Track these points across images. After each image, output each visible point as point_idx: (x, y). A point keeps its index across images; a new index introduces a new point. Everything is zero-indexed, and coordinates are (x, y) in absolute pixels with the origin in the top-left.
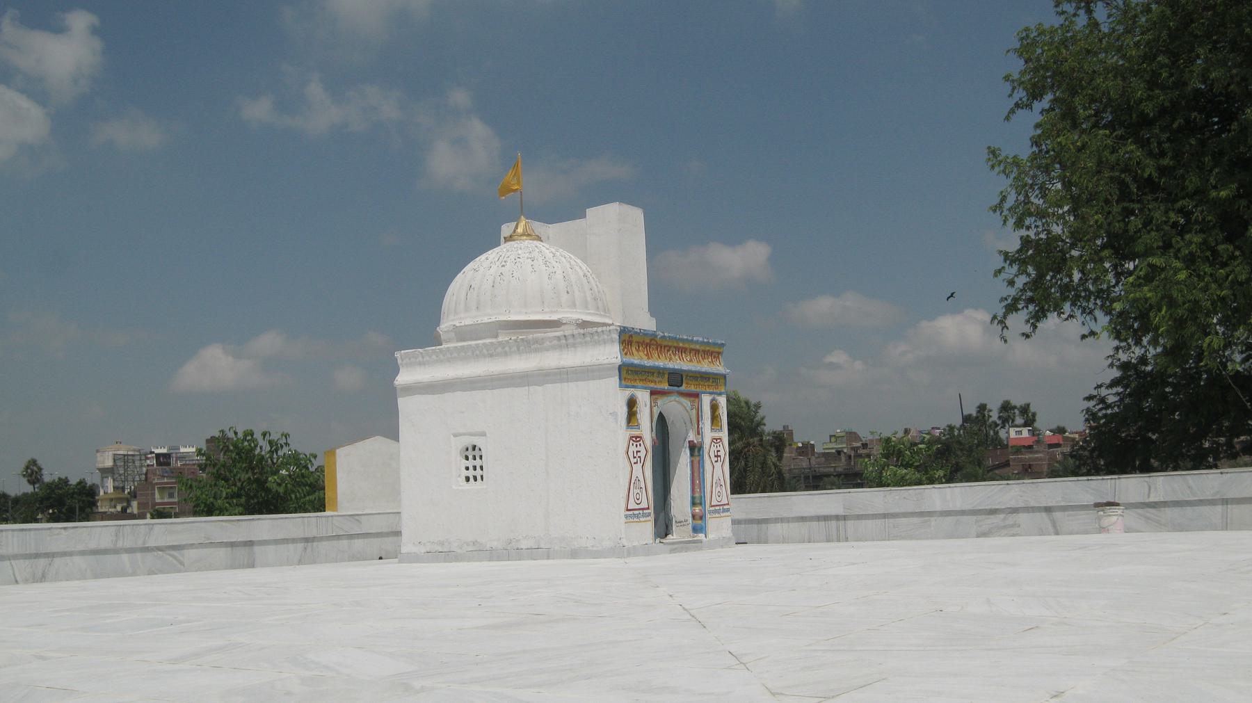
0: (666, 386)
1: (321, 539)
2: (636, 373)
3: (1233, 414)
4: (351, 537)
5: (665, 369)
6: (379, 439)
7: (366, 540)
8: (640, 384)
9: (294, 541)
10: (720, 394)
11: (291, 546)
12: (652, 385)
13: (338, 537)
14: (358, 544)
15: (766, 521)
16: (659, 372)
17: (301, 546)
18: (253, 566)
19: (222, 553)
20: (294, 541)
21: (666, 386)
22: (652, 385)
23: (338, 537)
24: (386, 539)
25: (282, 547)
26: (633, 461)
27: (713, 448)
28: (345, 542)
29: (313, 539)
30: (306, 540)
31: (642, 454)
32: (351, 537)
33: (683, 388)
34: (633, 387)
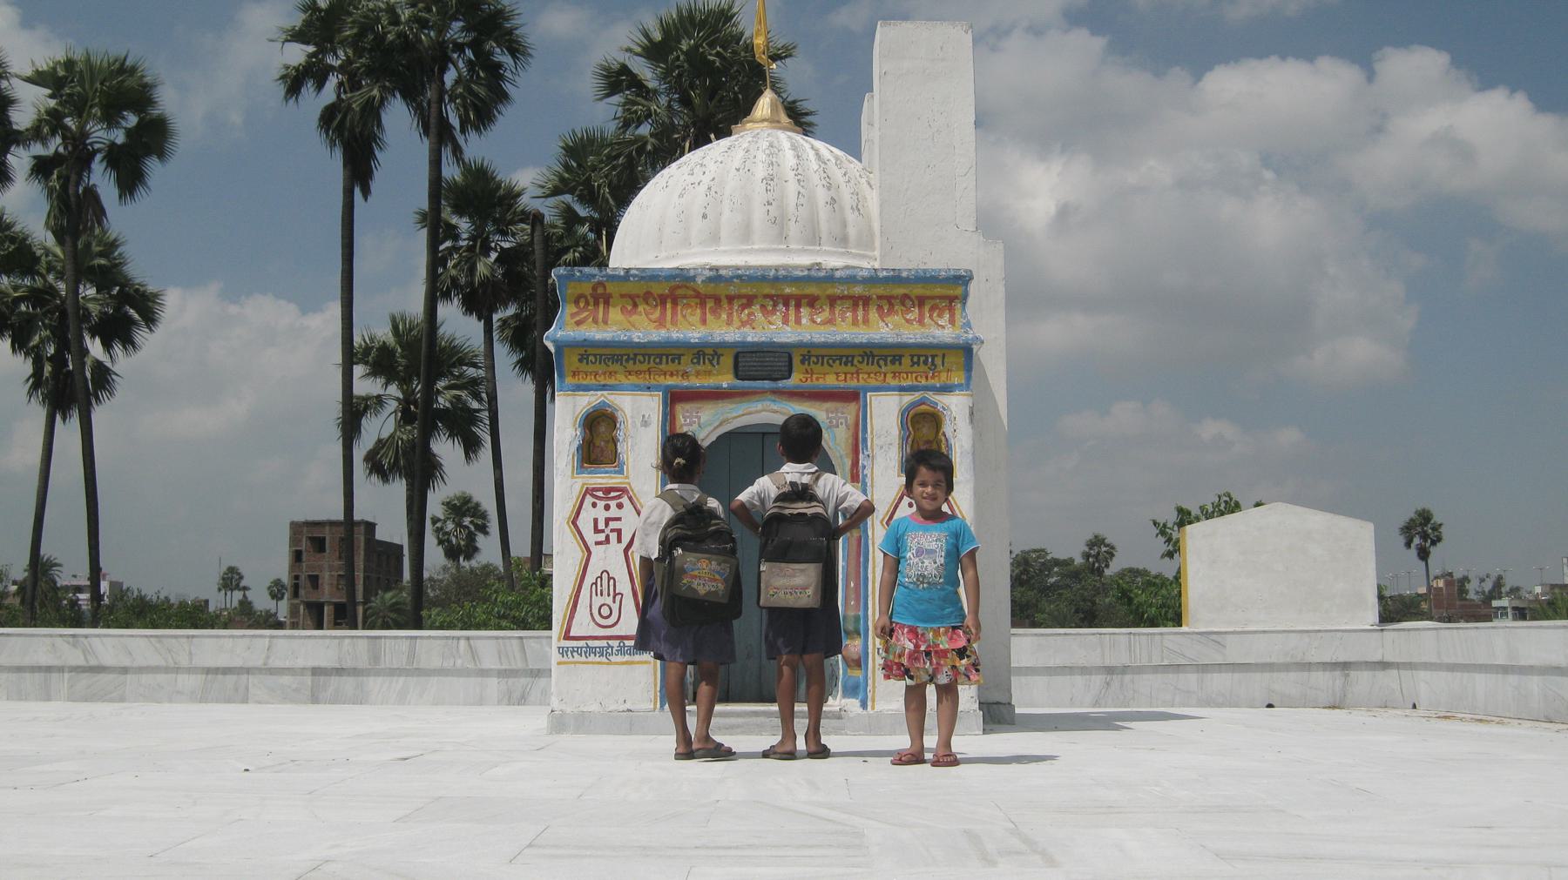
0: (726, 381)
1: (1140, 670)
2: (616, 359)
3: (1041, 189)
4: (1204, 668)
5: (724, 345)
7: (1237, 676)
8: (621, 378)
9: (1084, 670)
10: (946, 389)
11: (1079, 680)
13: (1177, 668)
14: (1219, 681)
17: (1098, 680)
20: (1084, 670)
21: (726, 381)
23: (1177, 668)
24: (1283, 675)
26: (591, 537)
27: (587, 515)
28: (1192, 678)
29: (1125, 670)
30: (1110, 670)
32: (1204, 668)
33: (795, 380)
34: (604, 387)
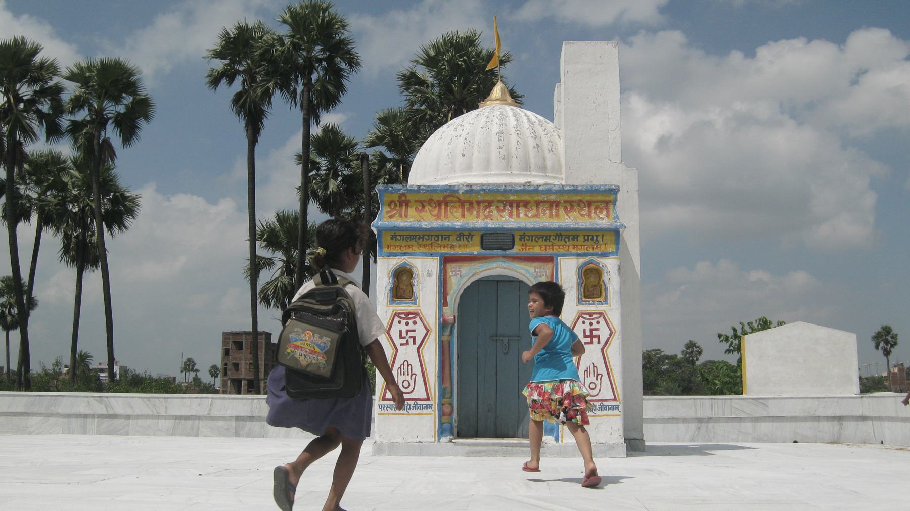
0: (476, 250)
1: (718, 420)
2: (413, 237)
4: (756, 420)
6: (801, 324)
7: (775, 424)
8: (416, 249)
9: (685, 420)
11: (682, 426)
12: (444, 251)
13: (740, 419)
14: (765, 427)
15: (879, 419)
16: (464, 234)
17: (693, 426)
18: (197, 435)
19: (168, 423)
20: (685, 420)
21: (476, 250)
22: (439, 250)
23: (740, 419)
25: (671, 426)
29: (709, 420)
30: (700, 420)
31: (420, 333)
32: (756, 420)
33: (516, 250)
34: (405, 254)
